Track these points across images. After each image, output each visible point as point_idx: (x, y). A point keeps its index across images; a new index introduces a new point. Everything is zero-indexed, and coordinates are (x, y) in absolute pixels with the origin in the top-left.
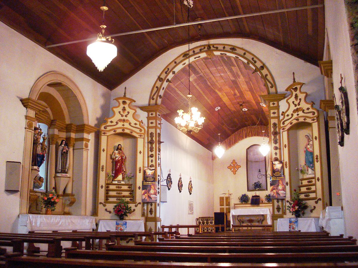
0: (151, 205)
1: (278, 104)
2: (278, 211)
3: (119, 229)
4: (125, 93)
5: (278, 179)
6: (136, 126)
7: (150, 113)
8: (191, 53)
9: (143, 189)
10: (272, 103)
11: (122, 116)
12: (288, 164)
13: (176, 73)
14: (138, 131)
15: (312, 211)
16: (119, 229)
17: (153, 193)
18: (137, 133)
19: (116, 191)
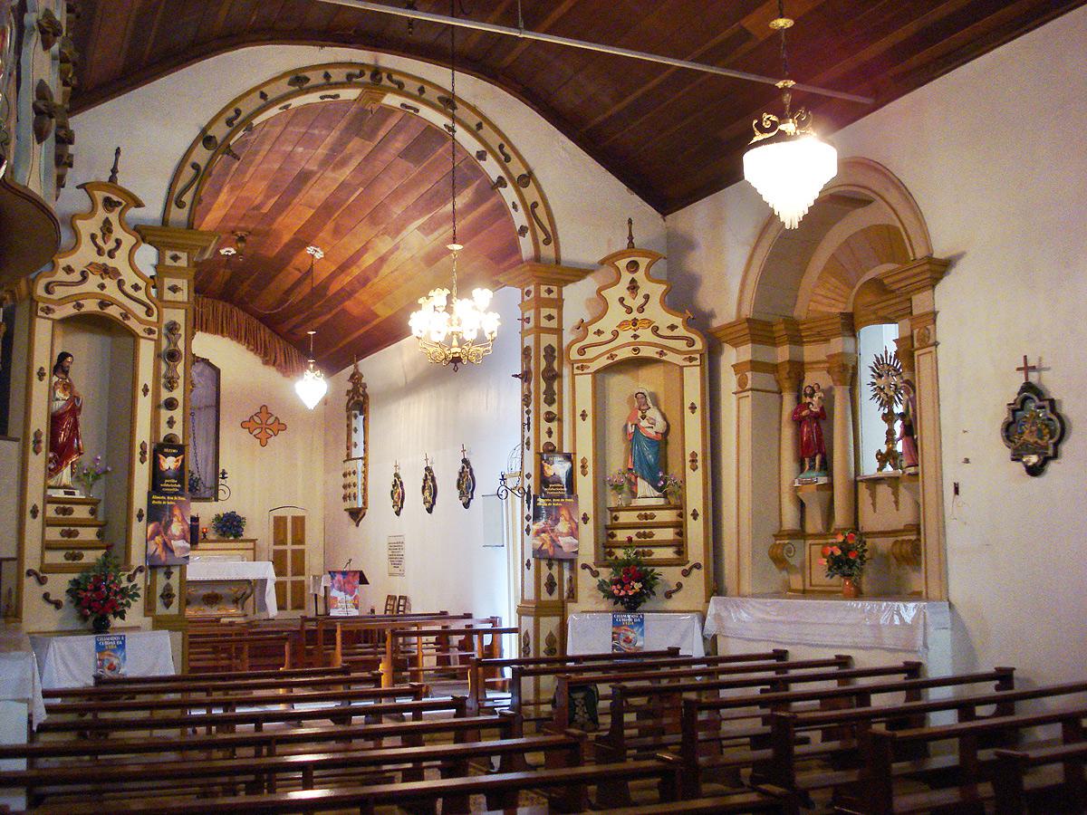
0: (168, 575)
1: (560, 293)
2: (550, 592)
3: (622, 637)
4: (114, 171)
5: (556, 502)
6: (676, 333)
7: (169, 253)
8: (316, 78)
9: (150, 520)
10: (546, 287)
11: (100, 252)
12: (137, 456)
13: (481, 162)
14: (681, 345)
15: (668, 595)
16: (622, 637)
17: (178, 533)
18: (141, 321)
19: (60, 526)
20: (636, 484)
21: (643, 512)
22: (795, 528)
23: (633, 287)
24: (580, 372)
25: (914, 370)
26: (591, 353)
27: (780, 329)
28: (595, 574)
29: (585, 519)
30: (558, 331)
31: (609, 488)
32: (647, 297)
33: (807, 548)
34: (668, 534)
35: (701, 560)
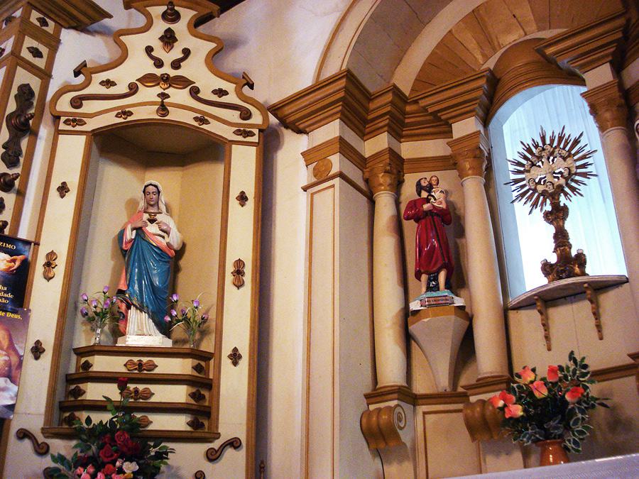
6: (224, 99)
14: (234, 116)
20: (125, 317)
21: (136, 359)
22: (396, 380)
23: (169, 39)
24: (69, 128)
25: (430, 262)
26: (89, 107)
27: (381, 104)
28: (42, 450)
29: (37, 351)
30: (45, 75)
31: (80, 318)
32: (187, 52)
33: (420, 418)
34: (179, 394)
35: (242, 435)
